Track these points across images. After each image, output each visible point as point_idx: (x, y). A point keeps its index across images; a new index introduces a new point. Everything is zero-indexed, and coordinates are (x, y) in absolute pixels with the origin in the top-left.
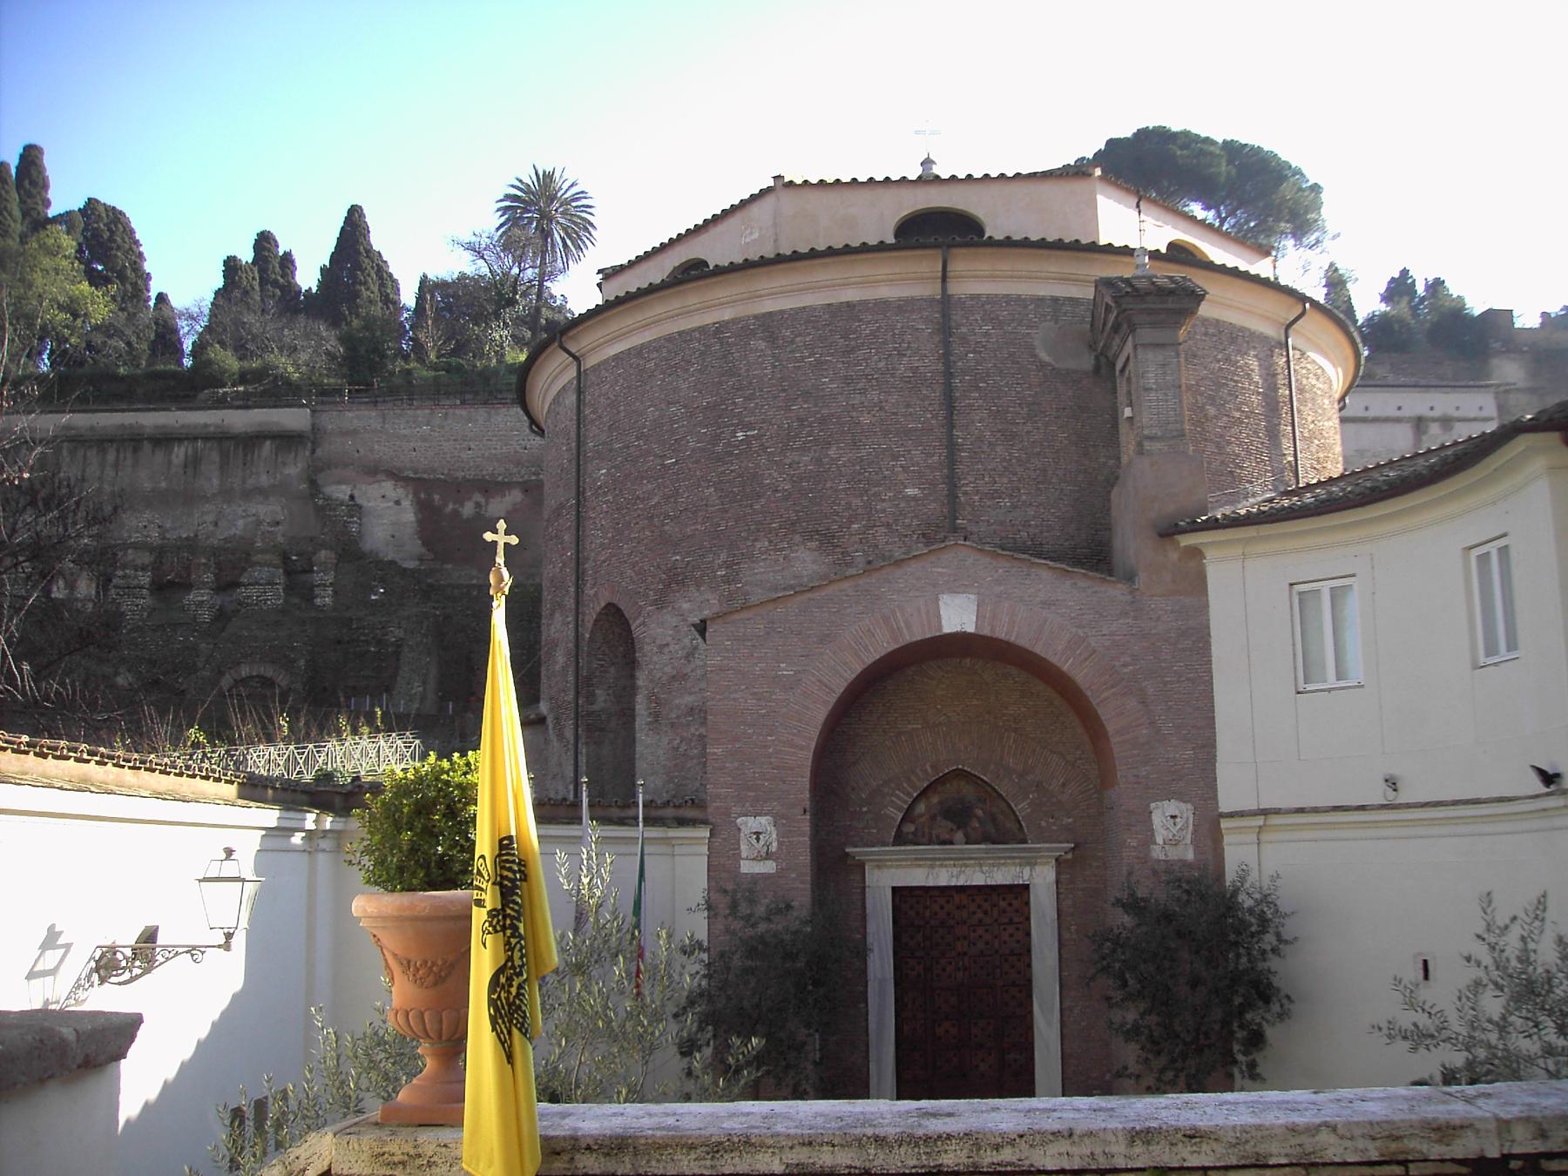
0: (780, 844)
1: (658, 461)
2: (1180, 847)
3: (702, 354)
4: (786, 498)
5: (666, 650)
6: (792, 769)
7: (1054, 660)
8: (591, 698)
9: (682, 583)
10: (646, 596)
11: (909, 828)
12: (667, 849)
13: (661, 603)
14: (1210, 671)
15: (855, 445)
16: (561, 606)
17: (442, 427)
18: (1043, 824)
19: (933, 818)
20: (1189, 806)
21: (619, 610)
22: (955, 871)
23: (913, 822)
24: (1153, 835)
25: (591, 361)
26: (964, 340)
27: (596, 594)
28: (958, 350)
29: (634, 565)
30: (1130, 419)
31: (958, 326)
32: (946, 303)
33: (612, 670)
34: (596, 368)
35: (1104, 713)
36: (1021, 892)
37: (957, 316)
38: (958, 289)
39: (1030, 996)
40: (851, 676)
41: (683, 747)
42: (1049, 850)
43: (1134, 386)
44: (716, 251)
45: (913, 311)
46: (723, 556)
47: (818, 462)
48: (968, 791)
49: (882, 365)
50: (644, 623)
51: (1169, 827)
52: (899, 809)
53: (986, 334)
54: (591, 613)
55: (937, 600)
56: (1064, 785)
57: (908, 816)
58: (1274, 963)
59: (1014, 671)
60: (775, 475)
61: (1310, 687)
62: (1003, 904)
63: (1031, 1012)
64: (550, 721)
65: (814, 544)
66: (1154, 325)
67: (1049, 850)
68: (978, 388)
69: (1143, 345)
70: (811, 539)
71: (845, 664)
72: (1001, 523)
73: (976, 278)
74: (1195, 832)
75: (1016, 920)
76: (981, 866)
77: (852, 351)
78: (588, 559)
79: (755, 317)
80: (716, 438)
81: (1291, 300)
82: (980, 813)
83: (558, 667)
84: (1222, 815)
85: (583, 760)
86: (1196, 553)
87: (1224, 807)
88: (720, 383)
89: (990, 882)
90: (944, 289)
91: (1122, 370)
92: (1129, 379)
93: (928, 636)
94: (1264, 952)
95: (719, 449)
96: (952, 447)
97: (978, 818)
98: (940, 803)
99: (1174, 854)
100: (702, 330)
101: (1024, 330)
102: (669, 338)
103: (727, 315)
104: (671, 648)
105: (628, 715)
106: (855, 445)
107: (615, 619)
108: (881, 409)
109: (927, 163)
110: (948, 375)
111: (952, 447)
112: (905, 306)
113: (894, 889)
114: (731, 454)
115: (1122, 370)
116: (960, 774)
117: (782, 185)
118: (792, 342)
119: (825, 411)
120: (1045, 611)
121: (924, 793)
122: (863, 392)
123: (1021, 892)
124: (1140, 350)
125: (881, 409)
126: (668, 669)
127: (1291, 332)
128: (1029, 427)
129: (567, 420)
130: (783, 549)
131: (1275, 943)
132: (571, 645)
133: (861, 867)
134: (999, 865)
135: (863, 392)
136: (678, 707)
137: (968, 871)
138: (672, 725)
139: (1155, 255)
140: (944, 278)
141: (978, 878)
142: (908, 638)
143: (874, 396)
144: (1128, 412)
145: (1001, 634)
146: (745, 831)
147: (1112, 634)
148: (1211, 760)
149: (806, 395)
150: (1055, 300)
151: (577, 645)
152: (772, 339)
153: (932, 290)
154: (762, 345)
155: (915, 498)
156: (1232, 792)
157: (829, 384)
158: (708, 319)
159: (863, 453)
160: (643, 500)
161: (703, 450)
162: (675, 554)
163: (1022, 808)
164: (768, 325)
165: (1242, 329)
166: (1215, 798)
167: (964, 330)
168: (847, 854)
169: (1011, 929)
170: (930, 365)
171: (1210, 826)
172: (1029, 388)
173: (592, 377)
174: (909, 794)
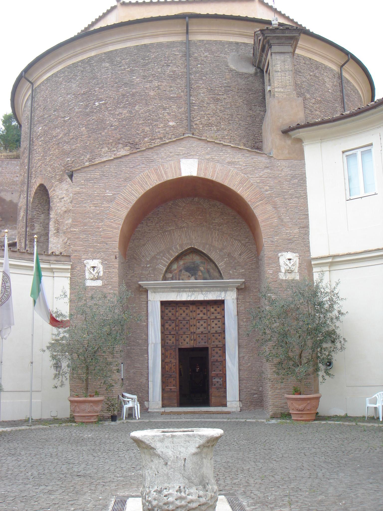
0: (104, 273)
1: (63, 119)
2: (293, 274)
4: (115, 129)
5: (63, 200)
6: (111, 238)
7: (233, 188)
12: (51, 274)
15: (147, 105)
17: (6, 168)
18: (231, 272)
19: (181, 271)
20: (297, 254)
21: (45, 187)
22: (190, 294)
23: (171, 273)
24: (280, 268)
26: (196, 59)
28: (193, 63)
30: (270, 91)
31: (194, 53)
32: (188, 44)
33: (42, 215)
36: (164, 304)
37: (193, 49)
38: (194, 38)
39: (225, 352)
40: (138, 196)
45: (173, 47)
46: (88, 156)
47: (130, 112)
48: (197, 259)
49: (159, 70)
50: (54, 190)
51: (287, 264)
52: (165, 266)
55: (180, 161)
56: (240, 255)
58: (338, 324)
59: (218, 203)
60: (112, 119)
62: (212, 310)
63: (225, 360)
66: (280, 44)
68: (202, 79)
69: (275, 53)
70: (126, 146)
74: (300, 267)
76: (202, 292)
78: (33, 167)
80: (87, 106)
81: (343, 54)
82: (202, 268)
87: (313, 255)
88: (89, 83)
89: (206, 299)
90: (187, 38)
91: (266, 72)
92: (269, 73)
93: (175, 177)
94: (332, 319)
95: (88, 110)
96: (190, 105)
97: (202, 272)
98: (184, 264)
99: (290, 277)
100: (82, 61)
101: (223, 55)
103: (93, 54)
104: (65, 199)
106: (147, 105)
107: (43, 191)
108: (159, 89)
111: (190, 105)
114: (93, 112)
115: (266, 72)
116: (193, 251)
118: (121, 62)
119: (134, 91)
122: (151, 82)
124: (273, 55)
125: (159, 89)
127: (342, 69)
128: (225, 96)
131: (337, 314)
134: (210, 291)
135: (151, 82)
136: (67, 224)
138: (64, 232)
140: (187, 33)
143: (156, 83)
144: (269, 88)
145: (209, 177)
146: (88, 266)
147: (261, 177)
148: (307, 234)
151: (27, 205)
152: (111, 62)
153: (180, 38)
154: (108, 65)
155: (173, 126)
156: (318, 249)
157: (136, 79)
160: (56, 137)
161: (81, 112)
162: (68, 158)
166: (309, 251)
169: (216, 321)
171: (307, 265)
172: (225, 80)
174: (169, 259)
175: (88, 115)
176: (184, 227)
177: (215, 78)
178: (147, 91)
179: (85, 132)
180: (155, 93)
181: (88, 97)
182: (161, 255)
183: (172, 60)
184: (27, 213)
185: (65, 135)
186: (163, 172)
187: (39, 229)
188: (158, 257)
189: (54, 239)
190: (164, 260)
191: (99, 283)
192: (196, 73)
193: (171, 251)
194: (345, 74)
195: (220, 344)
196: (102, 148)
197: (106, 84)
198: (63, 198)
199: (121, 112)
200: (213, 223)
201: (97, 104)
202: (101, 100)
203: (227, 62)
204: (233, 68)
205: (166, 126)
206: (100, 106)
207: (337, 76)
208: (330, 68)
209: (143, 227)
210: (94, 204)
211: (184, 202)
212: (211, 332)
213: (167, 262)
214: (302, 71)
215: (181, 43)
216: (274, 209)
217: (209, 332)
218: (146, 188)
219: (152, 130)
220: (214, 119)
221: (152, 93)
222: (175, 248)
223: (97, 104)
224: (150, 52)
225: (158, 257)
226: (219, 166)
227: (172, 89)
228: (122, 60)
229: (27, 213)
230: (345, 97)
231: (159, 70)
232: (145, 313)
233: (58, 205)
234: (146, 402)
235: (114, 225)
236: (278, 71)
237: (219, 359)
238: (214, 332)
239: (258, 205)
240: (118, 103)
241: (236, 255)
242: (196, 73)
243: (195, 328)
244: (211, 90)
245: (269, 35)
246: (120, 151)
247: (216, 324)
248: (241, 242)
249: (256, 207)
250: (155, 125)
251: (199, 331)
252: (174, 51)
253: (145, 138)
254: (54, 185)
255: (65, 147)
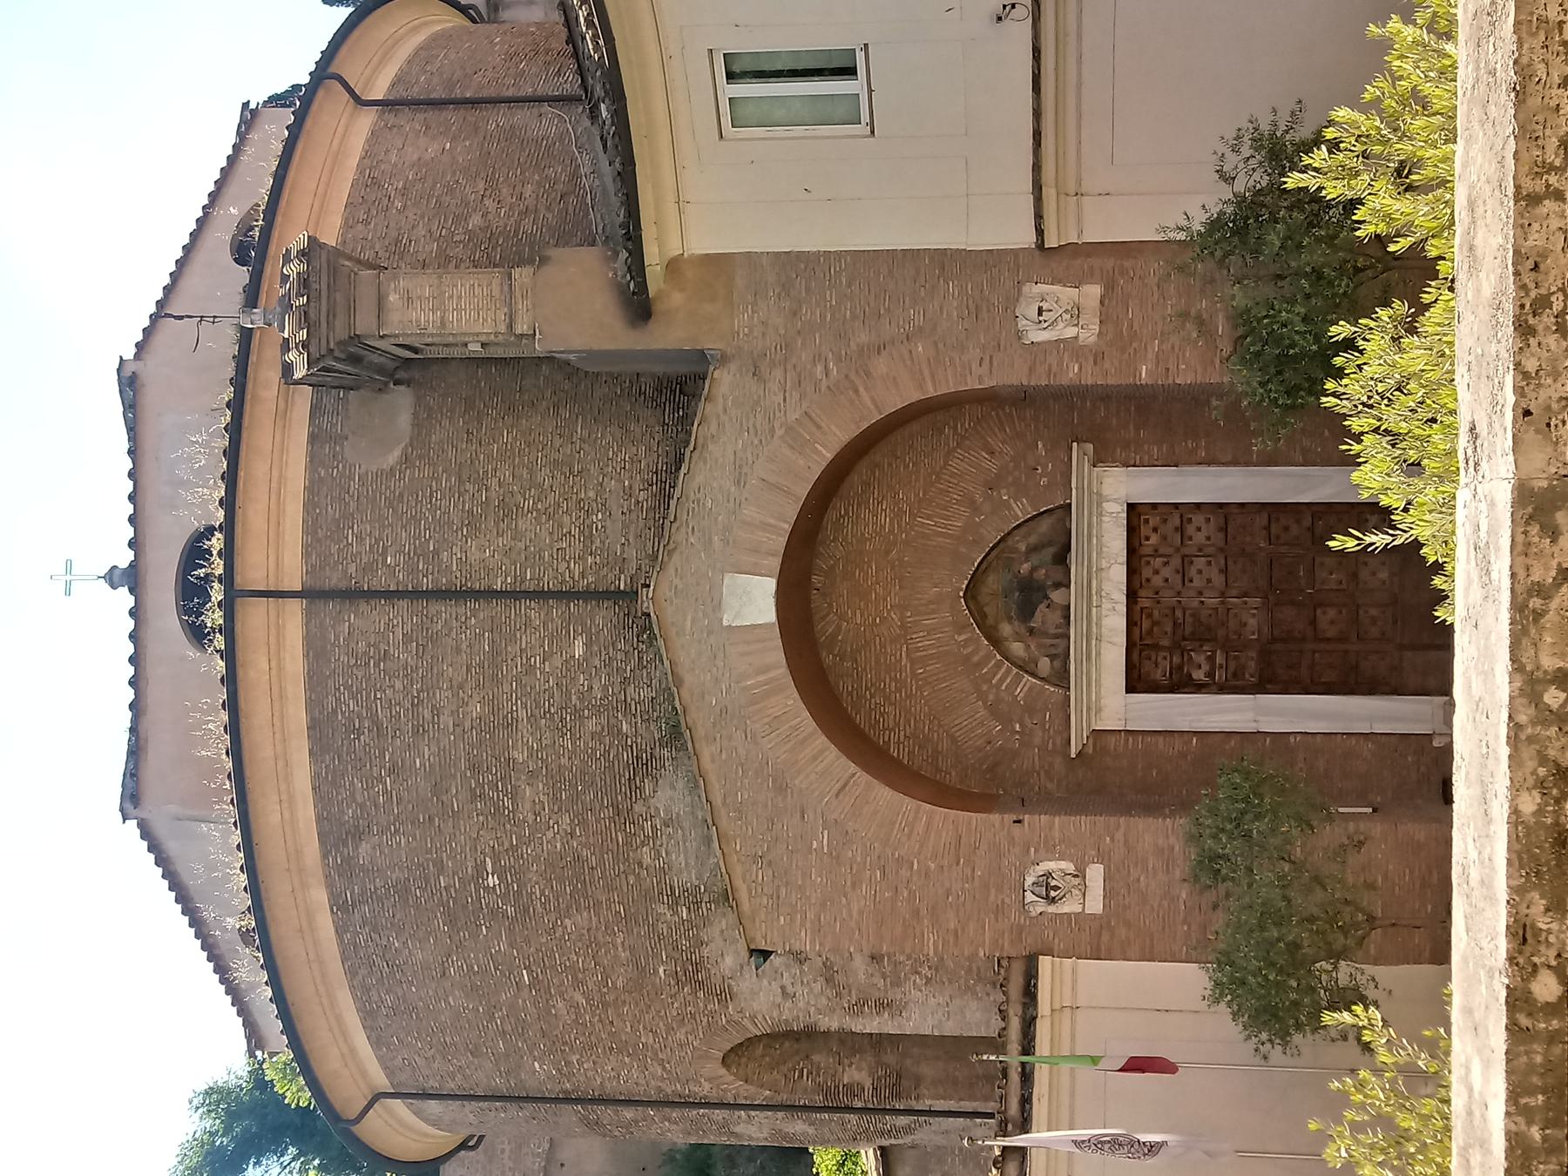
3: (374, 929)
4: (583, 823)
5: (790, 989)
7: (817, 471)
8: (853, 1090)
9: (698, 966)
10: (712, 1014)
11: (1044, 665)
13: (724, 995)
14: (840, 255)
16: (725, 1124)
19: (1031, 631)
22: (1106, 605)
25: (382, 1082)
27: (709, 1080)
29: (670, 1029)
34: (389, 1071)
35: (895, 402)
36: (1136, 682)
37: (334, 580)
40: (833, 752)
41: (925, 971)
42: (1080, 478)
43: (436, 340)
44: (233, 920)
46: (662, 909)
48: (993, 582)
49: (398, 685)
51: (1059, 322)
53: (360, 538)
54: (733, 1086)
56: (992, 453)
57: (1027, 667)
59: (831, 515)
61: (865, 117)
62: (1154, 539)
64: (885, 1143)
65: (648, 786)
66: (351, 309)
67: (1080, 478)
68: (436, 552)
70: (641, 789)
71: (815, 758)
72: (625, 526)
73: (277, 549)
75: (1177, 522)
76: (1100, 570)
77: (376, 723)
78: (660, 1090)
79: (325, 856)
82: (1025, 568)
83: (811, 1130)
84: (1040, 245)
85: (940, 1105)
86: (673, 266)
89: (1123, 558)
97: (1034, 569)
100: (340, 931)
102: (351, 973)
105: (878, 1042)
106: (511, 724)
108: (461, 687)
109: (113, 578)
110: (416, 594)
112: (315, 649)
113: (1131, 688)
114: (519, 892)
116: (971, 593)
117: (132, 797)
118: (362, 806)
120: (751, 467)
121: (996, 641)
123: (1136, 682)
125: (461, 687)
126: (817, 987)
129: (467, 1117)
130: (653, 827)
132: (780, 1114)
133: (1097, 734)
134: (1100, 546)
135: (436, 712)
137: (1107, 587)
139: (251, 297)
141: (1116, 576)
142: (781, 671)
143: (442, 696)
144: (475, 347)
149: (436, 789)
150: (313, 438)
152: (358, 835)
154: (365, 848)
155: (588, 645)
158: (325, 923)
159: (522, 714)
161: (510, 930)
162: (656, 971)
163: (1021, 510)
164: (336, 835)
165: (361, 169)
167: (352, 569)
168: (1079, 754)
169: (1190, 529)
170: (401, 616)
172: (439, 480)
173: (403, 1077)
174: (999, 665)
175: (526, 910)
176: (902, 619)
177: (433, 511)
178: (467, 725)
179: (582, 918)
180: (476, 698)
181: (465, 907)
182: (985, 688)
183: (369, 645)
184: (805, 1108)
185: (578, 983)
186: (761, 678)
187: (859, 1069)
188: (991, 697)
189: (908, 1020)
190: (1002, 680)
191: (1095, 873)
192: (413, 570)
193: (976, 659)
194: (379, 92)
195: (1261, 520)
196: (640, 864)
197: (429, 851)
198: (783, 988)
199: (528, 806)
200: (891, 531)
201: (492, 881)
202: (480, 869)
203: (380, 474)
204: (397, 453)
205: (584, 665)
206: (500, 872)
207: (391, 118)
208: (367, 141)
209: (899, 743)
210: (854, 884)
211: (823, 618)
212: (1222, 544)
213: (1008, 671)
214: (394, 234)
215: (309, 615)
216: (884, 353)
217: (1222, 550)
218: (810, 729)
219: (597, 710)
220: (566, 519)
221: (476, 709)
222: (965, 647)
223: (492, 881)
224: (334, 711)
225: (991, 697)
226: (749, 512)
227: (464, 646)
228: (354, 800)
229: (805, 1108)
230: (458, 93)
231: (398, 685)
232: (1161, 739)
233: (801, 1005)
234: (1435, 744)
235: (920, 827)
236: (442, 318)
237: (1307, 522)
238: (1221, 535)
239: (873, 399)
240: (498, 811)
241: (992, 466)
242: (413, 570)
243: (1207, 593)
244: (472, 523)
245: (324, 341)
246: (657, 809)
247: (1199, 529)
248: (954, 450)
249: (877, 407)
250: (581, 700)
251: (1218, 580)
252: (337, 637)
253: (620, 731)
254: (737, 1017)
255: (619, 984)
